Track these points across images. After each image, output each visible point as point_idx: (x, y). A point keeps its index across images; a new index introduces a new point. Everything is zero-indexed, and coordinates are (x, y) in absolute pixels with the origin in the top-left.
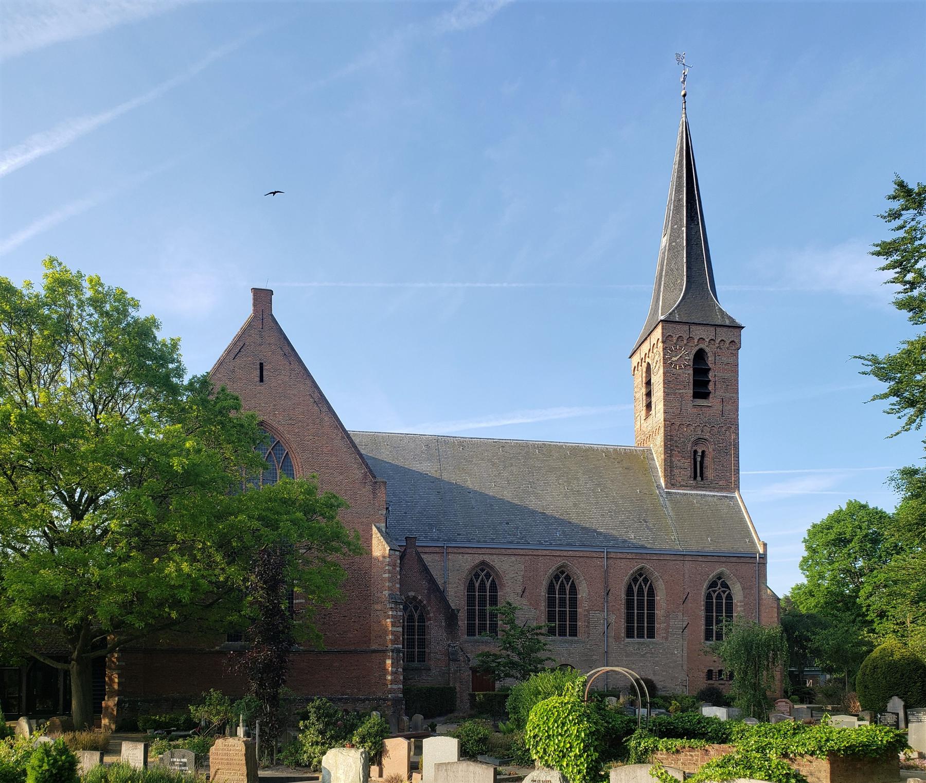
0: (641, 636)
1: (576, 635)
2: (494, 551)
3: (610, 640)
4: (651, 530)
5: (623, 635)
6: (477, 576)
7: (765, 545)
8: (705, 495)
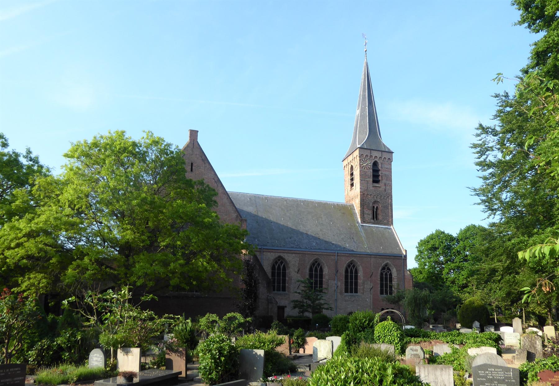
0: (351, 292)
4: (355, 243)
6: (276, 263)
7: (406, 251)
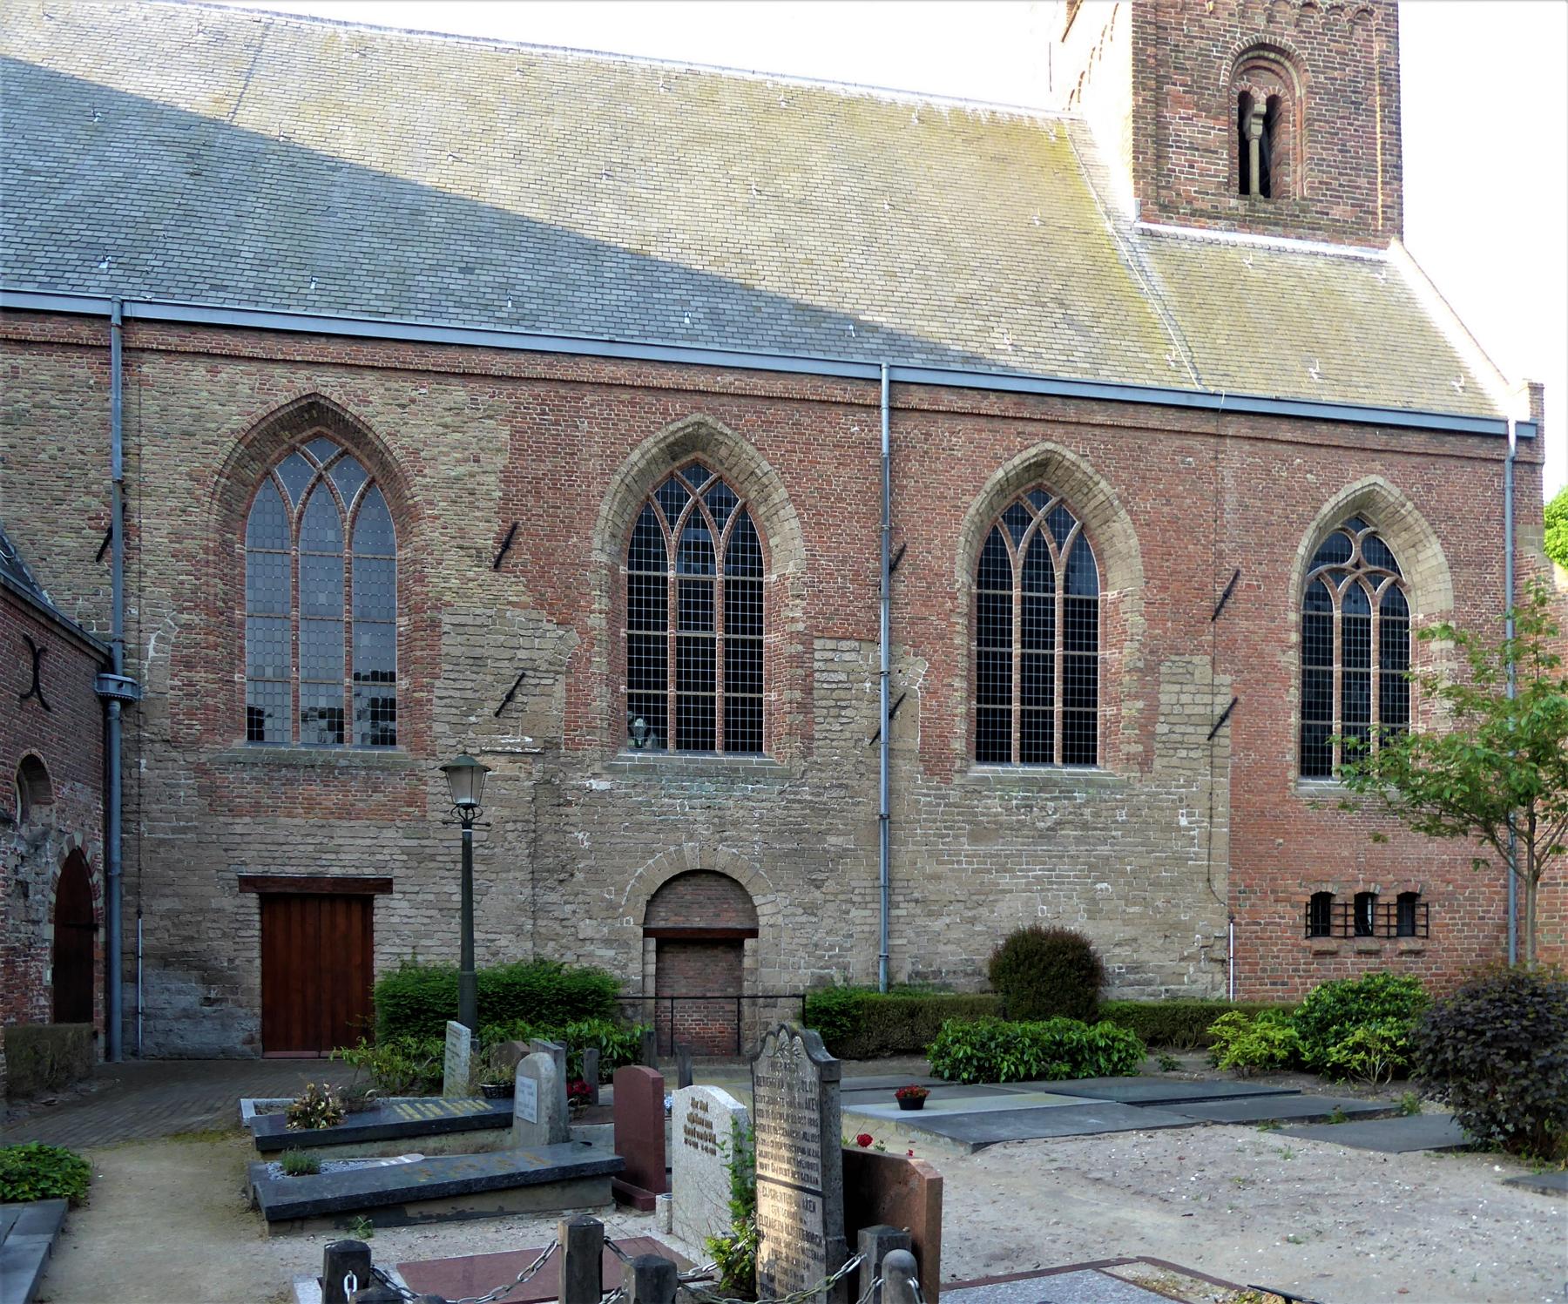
0: (1036, 752)
1: (756, 748)
2: (365, 354)
3: (905, 767)
4: (1083, 331)
5: (959, 745)
8: (1281, 251)
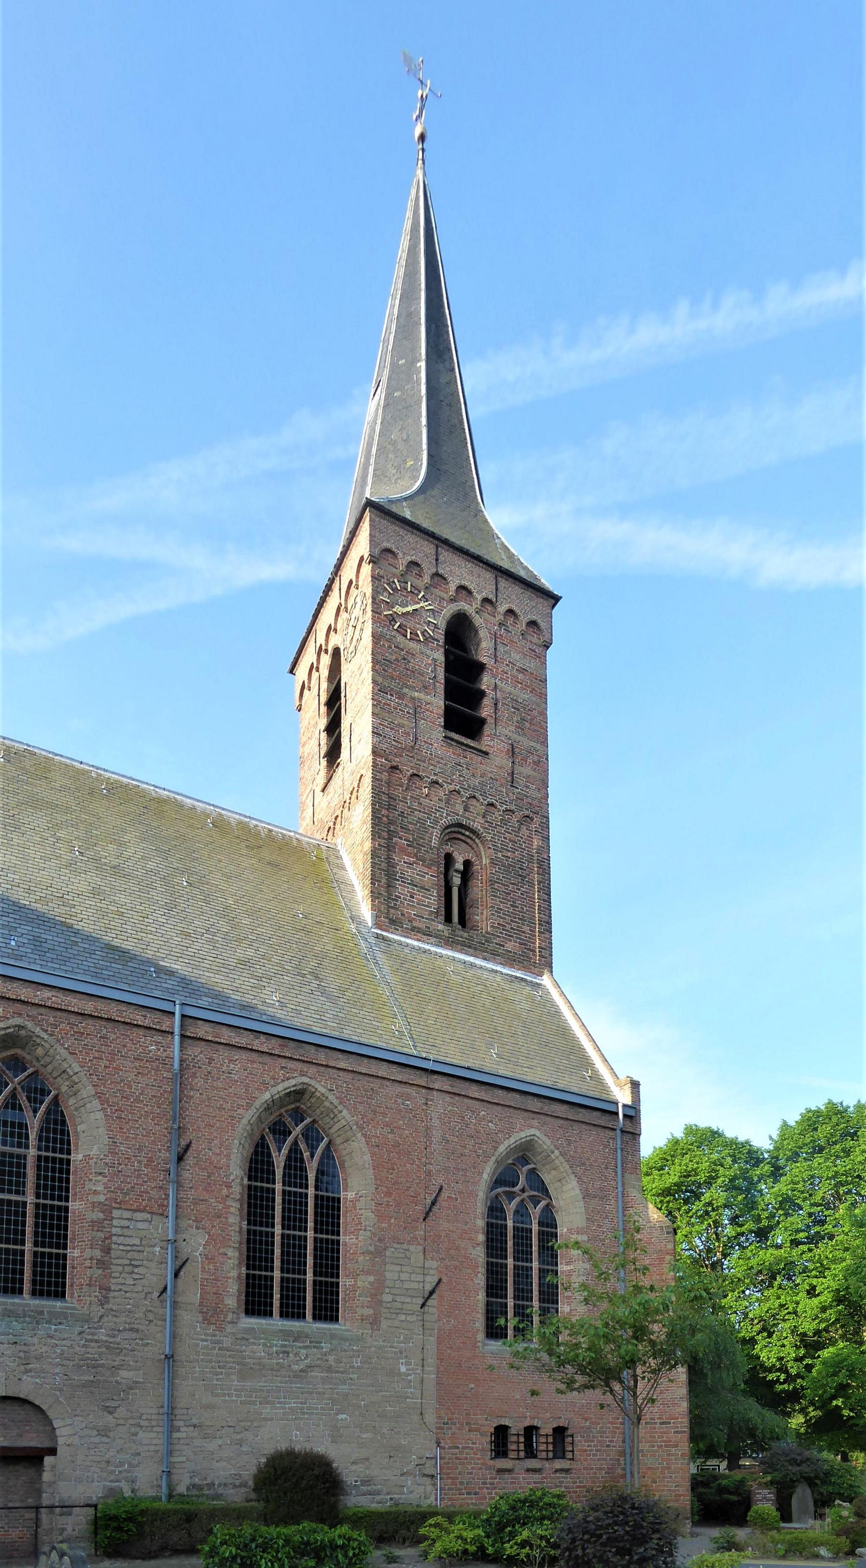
0: (292, 1309)
7: (635, 1086)
8: (472, 965)
